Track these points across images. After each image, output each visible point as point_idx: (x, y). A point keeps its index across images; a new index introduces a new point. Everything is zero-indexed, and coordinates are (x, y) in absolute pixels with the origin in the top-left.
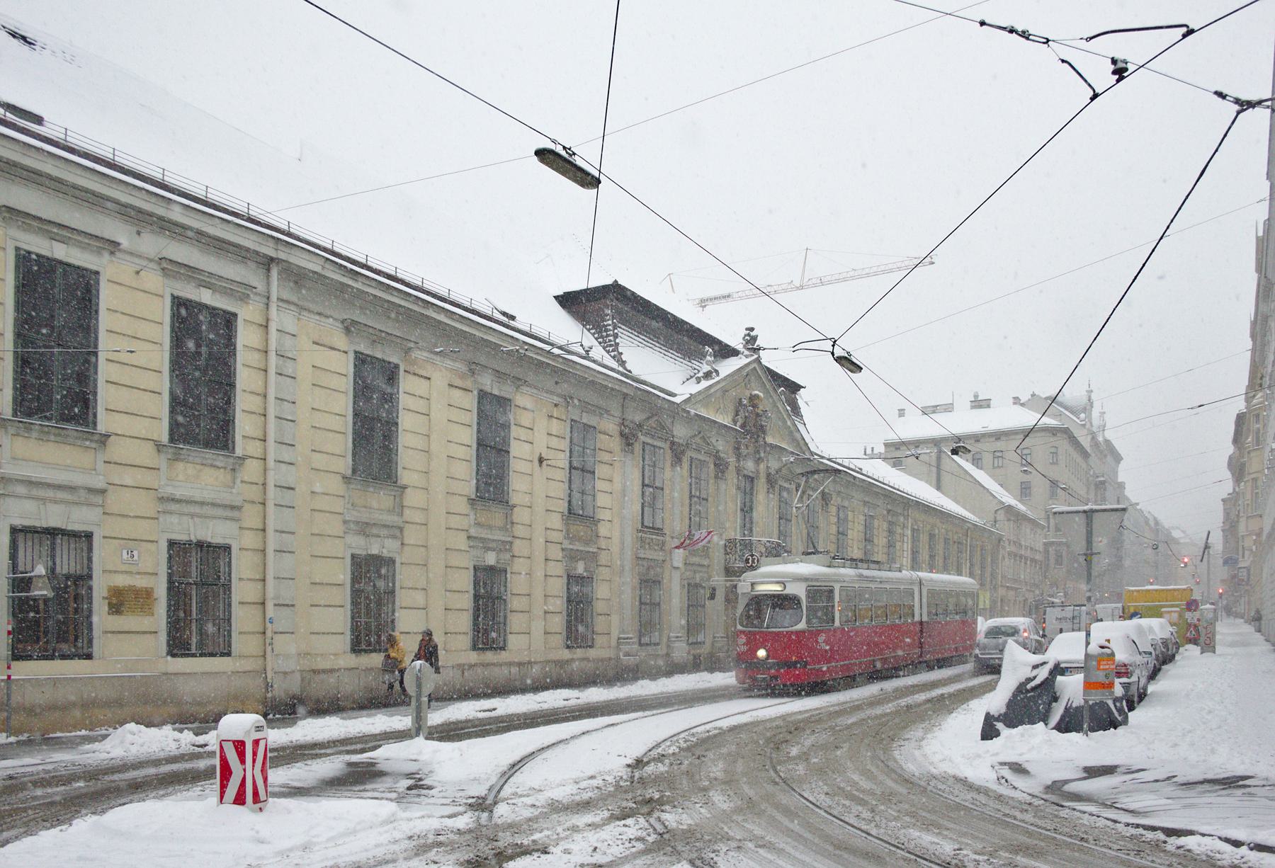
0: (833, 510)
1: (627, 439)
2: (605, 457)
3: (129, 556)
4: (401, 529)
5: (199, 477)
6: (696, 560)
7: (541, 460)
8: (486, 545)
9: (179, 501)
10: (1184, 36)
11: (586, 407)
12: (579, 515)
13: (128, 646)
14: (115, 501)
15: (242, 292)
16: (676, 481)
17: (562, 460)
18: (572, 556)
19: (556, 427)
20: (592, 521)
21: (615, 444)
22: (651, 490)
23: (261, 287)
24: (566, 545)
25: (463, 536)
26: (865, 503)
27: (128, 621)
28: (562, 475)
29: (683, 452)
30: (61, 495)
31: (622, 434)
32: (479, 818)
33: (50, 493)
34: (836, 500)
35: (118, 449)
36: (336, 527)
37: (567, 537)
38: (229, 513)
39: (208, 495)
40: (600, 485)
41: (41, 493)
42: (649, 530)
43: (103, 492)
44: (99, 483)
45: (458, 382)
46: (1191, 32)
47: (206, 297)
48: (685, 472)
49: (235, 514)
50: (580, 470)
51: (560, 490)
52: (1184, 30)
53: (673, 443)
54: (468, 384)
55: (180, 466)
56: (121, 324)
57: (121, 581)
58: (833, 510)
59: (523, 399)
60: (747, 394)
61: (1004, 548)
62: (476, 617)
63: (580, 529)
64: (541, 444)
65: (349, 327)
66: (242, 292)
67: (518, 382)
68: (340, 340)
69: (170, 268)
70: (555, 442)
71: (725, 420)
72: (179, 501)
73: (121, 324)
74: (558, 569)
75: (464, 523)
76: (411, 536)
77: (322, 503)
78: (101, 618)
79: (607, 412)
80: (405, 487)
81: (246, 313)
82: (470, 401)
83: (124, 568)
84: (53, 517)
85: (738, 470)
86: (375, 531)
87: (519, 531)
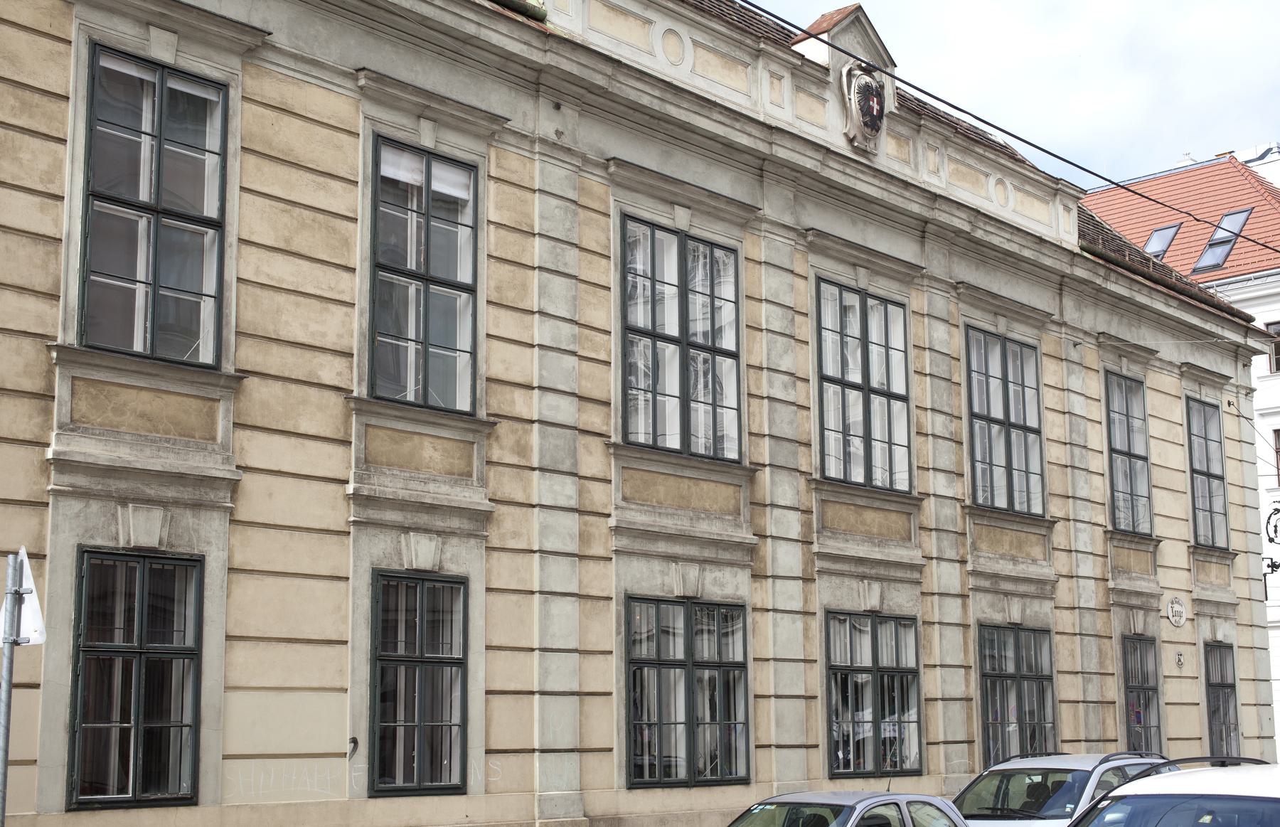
8: (637, 541)
15: (1040, 320)
40: (491, 320)
80: (1053, 523)
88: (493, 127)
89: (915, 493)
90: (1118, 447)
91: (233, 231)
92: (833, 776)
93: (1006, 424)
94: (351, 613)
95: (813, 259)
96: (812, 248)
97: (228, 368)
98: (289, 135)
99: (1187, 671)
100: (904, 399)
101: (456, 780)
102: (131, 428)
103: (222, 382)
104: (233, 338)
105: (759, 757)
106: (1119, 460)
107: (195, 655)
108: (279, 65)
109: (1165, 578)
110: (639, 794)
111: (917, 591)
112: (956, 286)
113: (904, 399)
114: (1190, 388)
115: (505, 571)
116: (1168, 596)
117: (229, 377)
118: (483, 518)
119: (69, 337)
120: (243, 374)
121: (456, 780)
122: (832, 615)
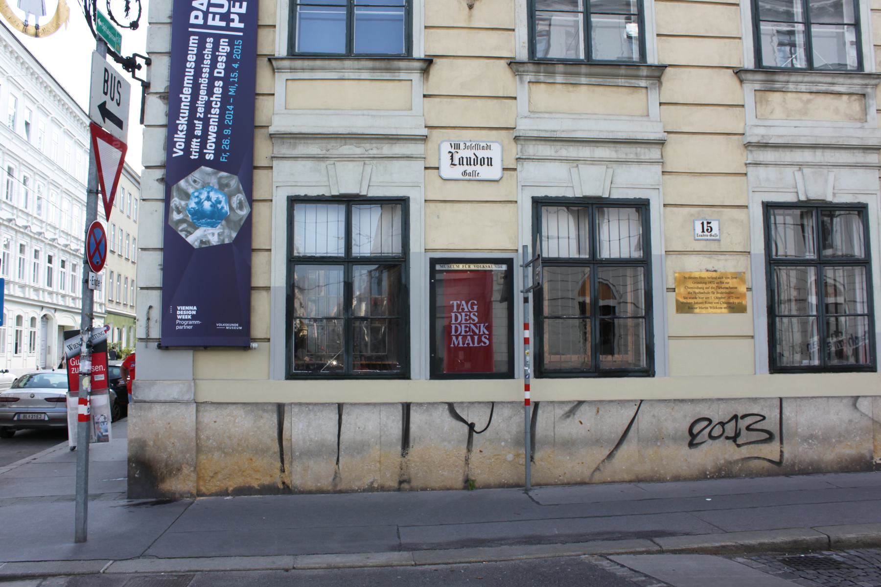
9: (776, 147)
33: (585, 152)
39: (825, 135)
41: (572, 152)
43: (661, 143)
44: (653, 131)
72: (776, 147)
83: (698, 246)
84: (590, 183)
108: (448, 545)
120: (662, 68)
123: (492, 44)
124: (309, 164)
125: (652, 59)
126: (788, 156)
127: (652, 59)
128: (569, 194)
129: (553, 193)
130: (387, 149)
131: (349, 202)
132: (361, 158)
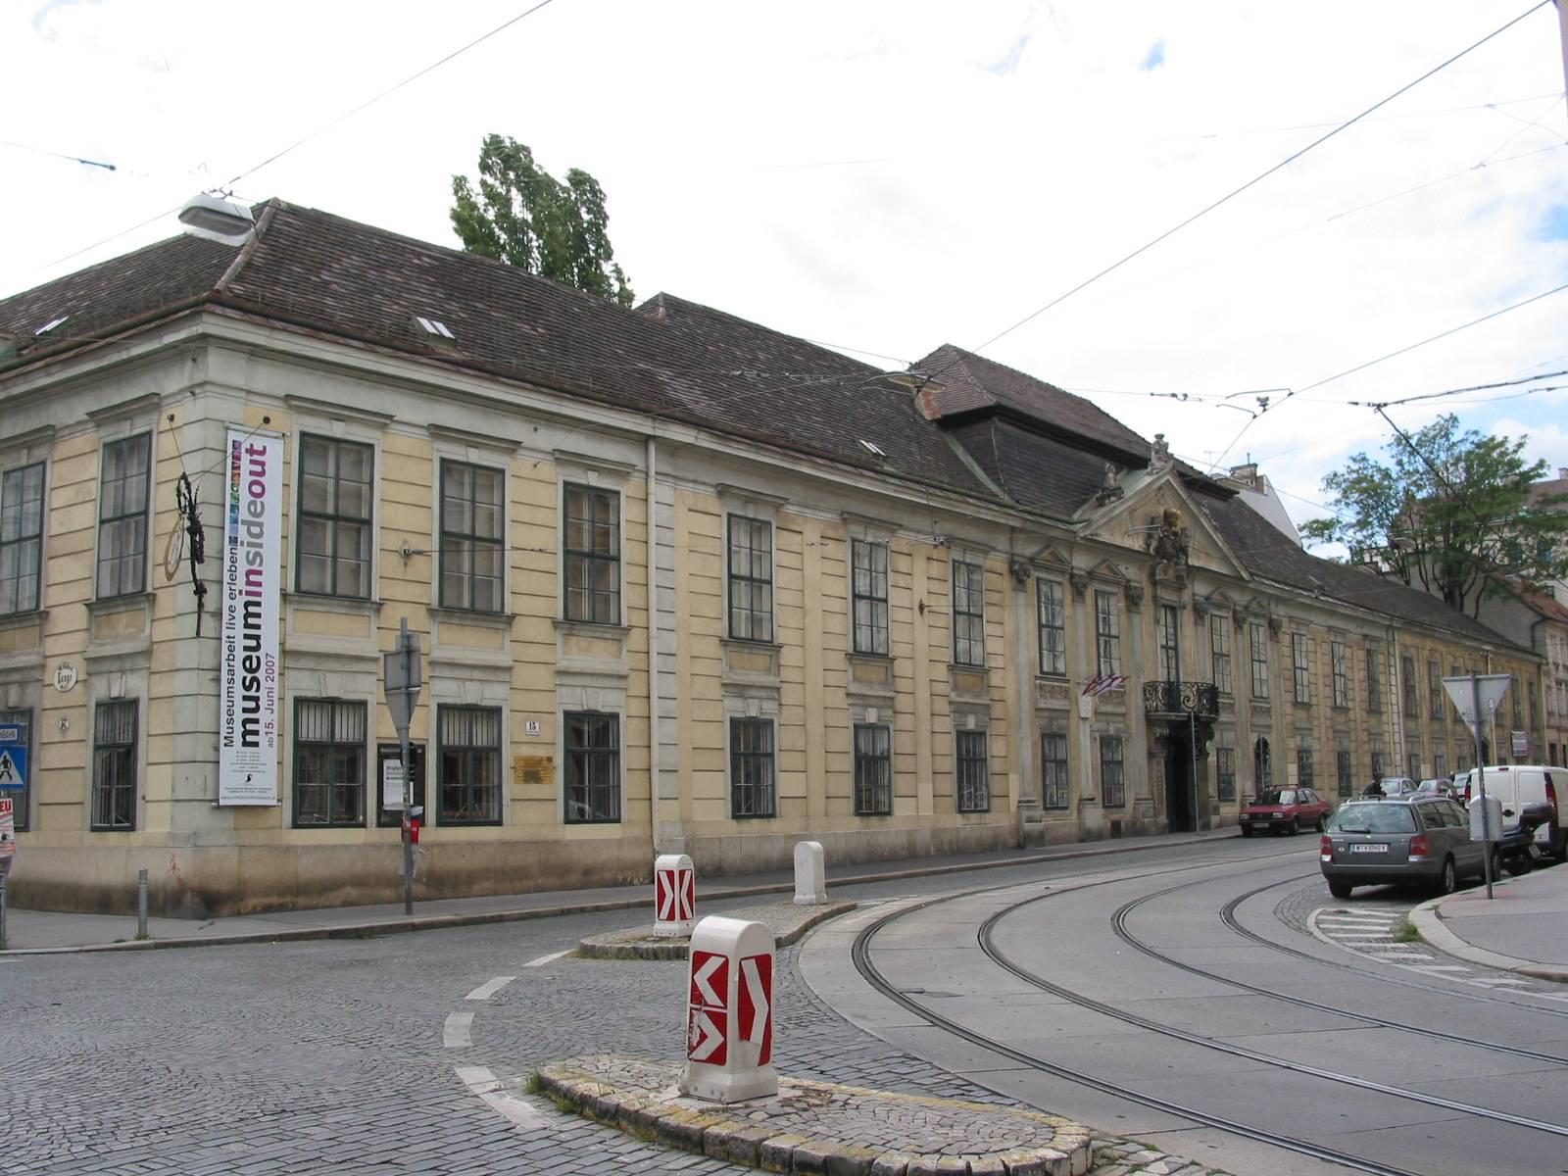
0: (1286, 640)
1: (1018, 576)
2: (995, 597)
3: (532, 733)
4: (778, 689)
5: (591, 654)
6: (1109, 708)
7: (921, 608)
8: (738, 690)
10: (1385, 405)
11: (967, 545)
12: (750, 638)
13: (532, 814)
14: (523, 676)
15: (622, 471)
16: (1078, 621)
17: (945, 605)
18: (960, 710)
19: (936, 569)
20: (981, 671)
21: (1006, 583)
22: (1049, 631)
23: (641, 465)
24: (953, 696)
25: (841, 693)
26: (1366, 637)
27: (534, 790)
28: (945, 621)
29: (1085, 586)
30: (477, 674)
31: (1012, 572)
32: (22, 694)
33: (466, 674)
34: (1286, 627)
35: (524, 629)
36: (716, 691)
37: (955, 688)
38: (616, 683)
40: (988, 629)
42: (1049, 679)
43: (509, 669)
44: (504, 660)
45: (831, 533)
46: (1379, 407)
47: (593, 479)
48: (1090, 609)
49: (622, 684)
50: (967, 617)
51: (942, 637)
52: (1383, 409)
53: (1072, 576)
54: (841, 534)
55: (573, 639)
56: (542, 516)
57: (526, 751)
58: (1286, 640)
59: (901, 541)
60: (1162, 510)
61: (1548, 674)
62: (735, 778)
63: (967, 680)
64: (921, 588)
65: (723, 491)
66: (622, 471)
67: (892, 527)
68: (712, 504)
69: (437, 432)
70: (936, 586)
71: (1137, 544)
73: (542, 516)
74: (946, 724)
75: (716, 668)
76: (789, 695)
77: (701, 667)
78: (511, 787)
79: (993, 549)
80: (629, 629)
81: (628, 489)
82: (843, 552)
85: (1155, 598)
86: (753, 693)
87: (903, 685)
88: (383, 421)
89: (775, 643)
90: (960, 609)
91: (890, 602)
92: (567, 821)
93: (473, 538)
94: (722, 737)
95: (561, 470)
96: (300, 410)
97: (375, 597)
98: (312, 719)
99: (72, 735)
100: (1306, 669)
101: (496, 817)
102: (752, 670)
103: (504, 619)
104: (1545, 716)
105: (896, 801)
106: (863, 607)
107: (616, 753)
109: (52, 646)
110: (376, 750)
111: (508, 686)
112: (288, 397)
113: (1306, 669)
114: (957, 555)
115: (160, 687)
116: (53, 663)
117: (624, 629)
118: (148, 653)
119: (560, 616)
120: (513, 616)
121: (496, 817)
122: (299, 702)
123: (415, 592)
124: (307, 673)
125: (508, 611)
126: (579, 681)
127: (508, 611)
128: (458, 701)
129: (450, 701)
130: (231, 393)
131: (333, 703)
132: (481, 681)
